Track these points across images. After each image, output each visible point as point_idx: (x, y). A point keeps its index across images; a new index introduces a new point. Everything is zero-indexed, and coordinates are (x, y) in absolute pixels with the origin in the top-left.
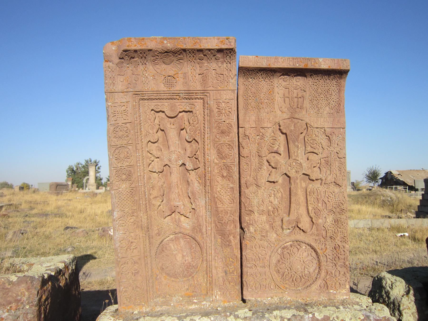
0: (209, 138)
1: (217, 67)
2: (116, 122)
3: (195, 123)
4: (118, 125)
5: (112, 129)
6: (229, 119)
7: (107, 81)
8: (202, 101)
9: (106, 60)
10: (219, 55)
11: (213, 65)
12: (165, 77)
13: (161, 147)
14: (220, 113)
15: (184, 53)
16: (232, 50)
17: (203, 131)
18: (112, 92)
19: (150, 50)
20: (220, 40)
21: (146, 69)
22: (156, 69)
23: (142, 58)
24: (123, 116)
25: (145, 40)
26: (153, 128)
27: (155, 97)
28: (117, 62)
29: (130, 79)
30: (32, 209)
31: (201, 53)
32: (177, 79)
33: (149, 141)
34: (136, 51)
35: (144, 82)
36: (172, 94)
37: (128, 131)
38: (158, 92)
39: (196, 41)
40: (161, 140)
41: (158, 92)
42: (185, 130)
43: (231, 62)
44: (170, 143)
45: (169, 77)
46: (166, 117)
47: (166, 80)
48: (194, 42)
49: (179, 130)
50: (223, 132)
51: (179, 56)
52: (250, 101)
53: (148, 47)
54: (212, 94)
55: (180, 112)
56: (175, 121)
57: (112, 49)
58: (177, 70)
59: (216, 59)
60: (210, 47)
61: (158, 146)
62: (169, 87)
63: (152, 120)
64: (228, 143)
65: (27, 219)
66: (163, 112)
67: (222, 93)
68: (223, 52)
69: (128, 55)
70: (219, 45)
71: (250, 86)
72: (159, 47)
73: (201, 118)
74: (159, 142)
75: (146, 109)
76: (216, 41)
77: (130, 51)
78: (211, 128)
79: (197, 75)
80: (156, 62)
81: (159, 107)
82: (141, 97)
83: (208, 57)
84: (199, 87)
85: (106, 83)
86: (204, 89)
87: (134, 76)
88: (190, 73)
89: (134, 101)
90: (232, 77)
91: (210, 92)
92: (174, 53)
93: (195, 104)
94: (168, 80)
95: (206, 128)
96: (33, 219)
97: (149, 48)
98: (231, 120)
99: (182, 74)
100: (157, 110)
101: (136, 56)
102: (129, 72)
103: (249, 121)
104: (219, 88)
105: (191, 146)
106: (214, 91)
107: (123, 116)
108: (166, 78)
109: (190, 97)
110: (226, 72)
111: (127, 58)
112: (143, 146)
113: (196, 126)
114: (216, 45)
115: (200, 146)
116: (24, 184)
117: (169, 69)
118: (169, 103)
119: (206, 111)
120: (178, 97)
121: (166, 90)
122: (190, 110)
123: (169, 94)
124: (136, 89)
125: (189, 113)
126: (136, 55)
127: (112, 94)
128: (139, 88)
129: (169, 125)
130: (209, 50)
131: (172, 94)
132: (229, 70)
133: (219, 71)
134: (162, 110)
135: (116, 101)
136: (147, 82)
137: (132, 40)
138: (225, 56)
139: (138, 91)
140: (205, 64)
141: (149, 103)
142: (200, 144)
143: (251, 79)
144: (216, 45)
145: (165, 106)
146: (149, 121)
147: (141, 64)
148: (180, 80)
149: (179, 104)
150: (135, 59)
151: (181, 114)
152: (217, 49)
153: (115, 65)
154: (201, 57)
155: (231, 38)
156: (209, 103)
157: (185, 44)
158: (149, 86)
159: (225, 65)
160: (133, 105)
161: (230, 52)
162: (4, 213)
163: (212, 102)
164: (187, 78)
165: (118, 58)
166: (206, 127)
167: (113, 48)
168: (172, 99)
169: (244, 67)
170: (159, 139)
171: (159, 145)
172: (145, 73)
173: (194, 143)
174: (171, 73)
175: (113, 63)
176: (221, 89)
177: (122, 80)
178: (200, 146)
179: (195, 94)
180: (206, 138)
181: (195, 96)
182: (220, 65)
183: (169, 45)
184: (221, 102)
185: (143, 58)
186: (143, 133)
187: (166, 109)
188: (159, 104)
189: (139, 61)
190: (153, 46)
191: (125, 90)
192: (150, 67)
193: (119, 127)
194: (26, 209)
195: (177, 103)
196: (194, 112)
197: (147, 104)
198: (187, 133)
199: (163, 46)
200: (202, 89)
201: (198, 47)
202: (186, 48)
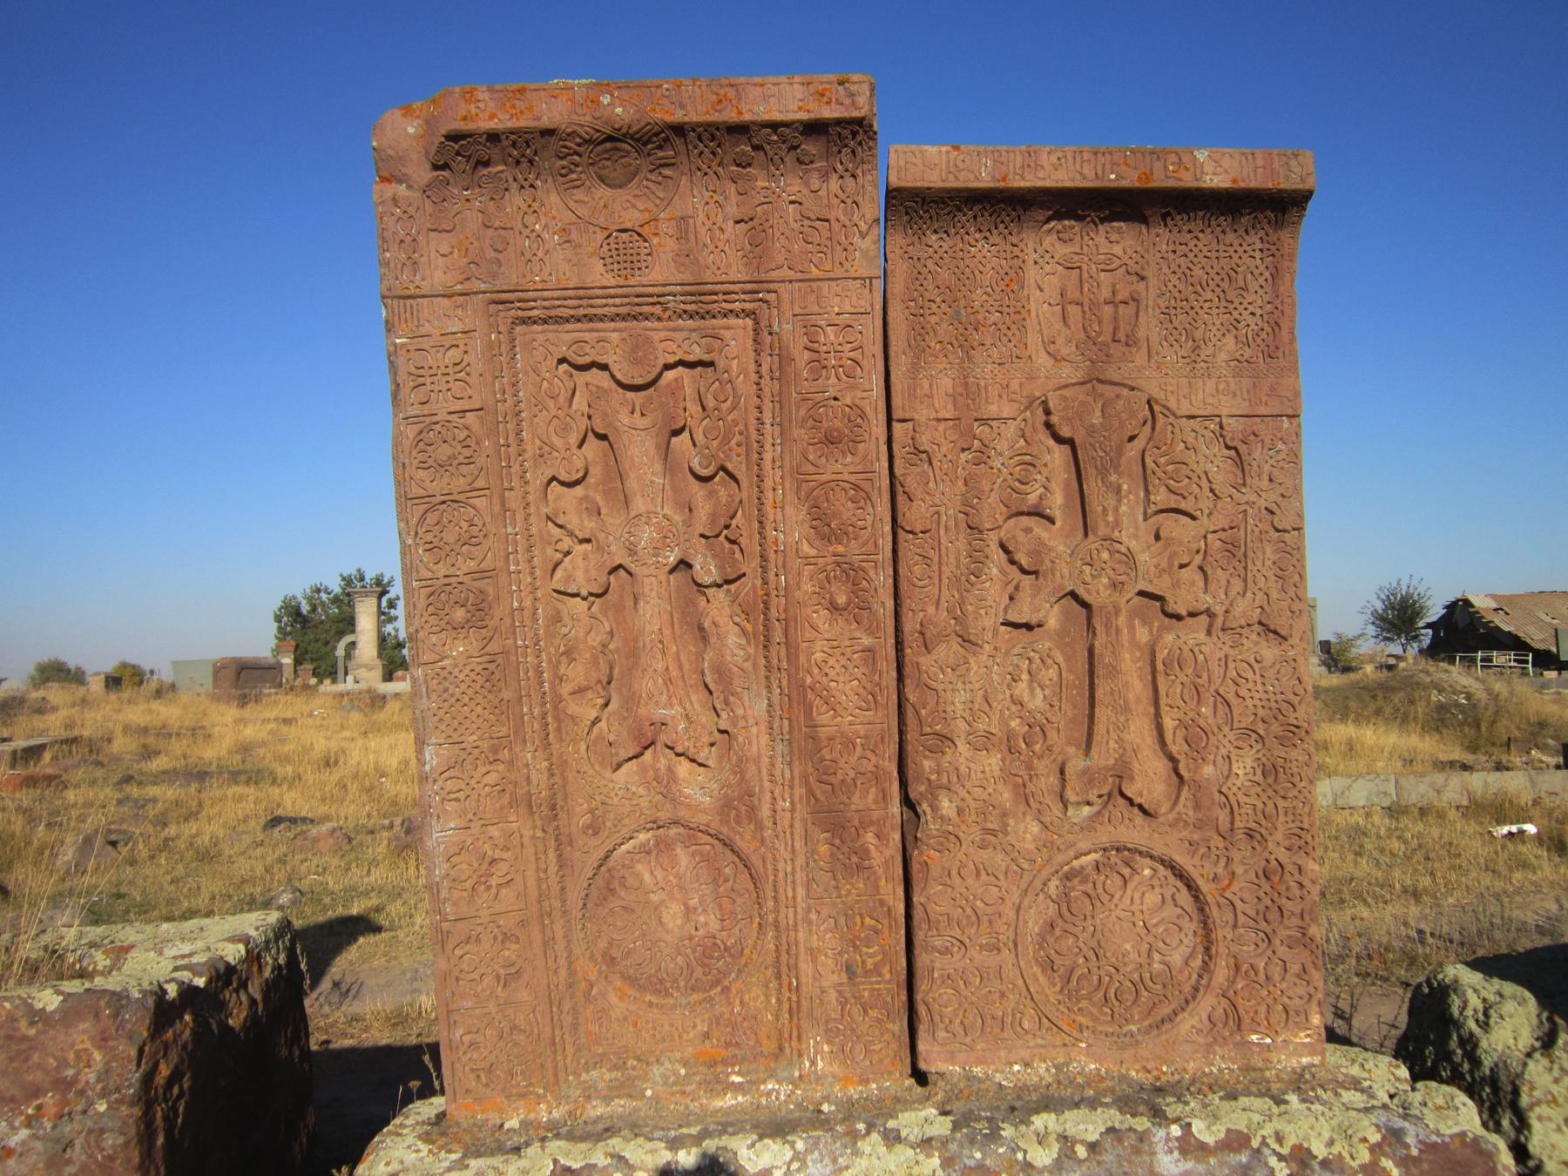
1: (805, 191)
2: (426, 410)
3: (724, 406)
4: (435, 419)
5: (411, 436)
6: (853, 387)
9: (385, 174)
10: (810, 147)
11: (791, 185)
12: (606, 234)
14: (819, 366)
15: (679, 142)
16: (861, 125)
17: (754, 435)
18: (409, 297)
19: (548, 133)
20: (812, 88)
22: (572, 204)
23: (518, 163)
26: (566, 429)
27: (572, 312)
28: (425, 182)
29: (476, 244)
30: (148, 753)
31: (744, 138)
32: (655, 241)
34: (493, 137)
35: (528, 255)
38: (581, 292)
39: (722, 92)
40: (596, 474)
41: (583, 293)
42: (686, 434)
43: (859, 172)
44: (632, 483)
46: (614, 386)
48: (715, 98)
50: (830, 440)
51: (660, 154)
53: (539, 119)
54: (786, 297)
57: (404, 131)
58: (650, 206)
60: (776, 116)
62: (623, 272)
63: (561, 399)
64: (852, 478)
65: (134, 791)
67: (825, 292)
69: (466, 154)
73: (745, 386)
74: (591, 480)
75: (540, 359)
76: (798, 91)
77: (471, 136)
78: (786, 424)
79: (731, 223)
80: (574, 176)
81: (587, 348)
82: (520, 313)
83: (770, 153)
86: (756, 276)
87: (490, 232)
88: (702, 216)
89: (491, 326)
92: (638, 140)
93: (727, 334)
94: (621, 246)
97: (546, 122)
98: (859, 394)
99: (673, 223)
100: (581, 361)
101: (495, 158)
102: (473, 218)
106: (797, 285)
108: (611, 240)
109: (702, 309)
112: (530, 498)
113: (730, 418)
114: (800, 109)
117: (624, 206)
118: (625, 335)
120: (657, 310)
121: (613, 282)
122: (706, 357)
124: (500, 284)
126: (495, 152)
127: (408, 302)
129: (625, 418)
130: (774, 126)
132: (849, 201)
134: (600, 359)
135: (423, 331)
136: (540, 254)
140: (760, 184)
143: (934, 237)
144: (800, 109)
145: (611, 343)
146: (551, 403)
147: (514, 186)
148: (666, 245)
149: (663, 334)
150: (493, 170)
151: (670, 375)
152: (801, 122)
154: (744, 153)
155: (855, 78)
156: (776, 328)
157: (682, 106)
159: (834, 184)
160: (490, 345)
161: (854, 134)
163: (790, 326)
164: (692, 237)
165: (428, 166)
167: (411, 130)
168: (635, 318)
170: (592, 471)
171: (591, 493)
172: (530, 219)
173: (722, 483)
174: (632, 218)
175: (409, 187)
176: (822, 275)
177: (445, 249)
178: (744, 495)
179: (721, 297)
180: (767, 464)
182: (815, 183)
183: (619, 110)
185: (525, 165)
186: (529, 447)
187: (615, 358)
188: (586, 336)
190: (559, 117)
191: (459, 287)
193: (438, 427)
195: (656, 332)
196: (721, 363)
197: (541, 338)
199: (597, 114)
201: (730, 115)
202: (686, 119)
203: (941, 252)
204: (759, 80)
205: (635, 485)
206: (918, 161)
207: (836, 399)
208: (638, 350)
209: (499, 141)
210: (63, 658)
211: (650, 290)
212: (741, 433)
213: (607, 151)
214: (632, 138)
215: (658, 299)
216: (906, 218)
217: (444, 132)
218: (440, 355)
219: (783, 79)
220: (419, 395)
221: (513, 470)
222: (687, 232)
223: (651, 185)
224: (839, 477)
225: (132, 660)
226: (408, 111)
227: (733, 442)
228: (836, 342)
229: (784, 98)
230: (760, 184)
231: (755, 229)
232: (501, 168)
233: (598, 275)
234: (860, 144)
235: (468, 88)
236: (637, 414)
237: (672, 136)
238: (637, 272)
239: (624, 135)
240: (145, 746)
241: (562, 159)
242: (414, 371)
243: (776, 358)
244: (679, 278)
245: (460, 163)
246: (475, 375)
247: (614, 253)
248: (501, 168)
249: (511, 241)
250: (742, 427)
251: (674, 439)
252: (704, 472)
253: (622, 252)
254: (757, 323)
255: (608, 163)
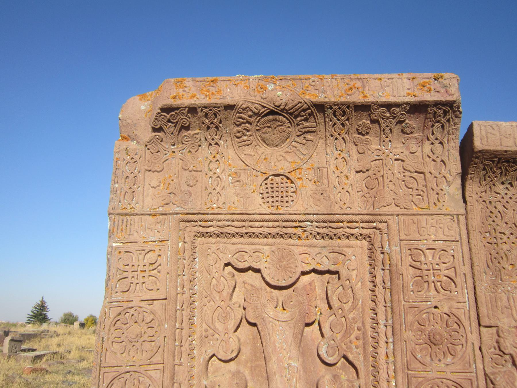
0: (391, 359)
1: (406, 152)
2: (125, 297)
3: (347, 307)
4: (131, 304)
5: (112, 316)
6: (450, 299)
7: (117, 185)
8: (365, 243)
9: (124, 135)
10: (412, 122)
11: (397, 147)
12: (265, 177)
13: (247, 372)
14: (422, 280)
15: (320, 116)
16: (451, 107)
17: (369, 331)
18: (126, 215)
19: (230, 107)
20: (416, 82)
21: (218, 157)
22: (243, 157)
23: (208, 128)
24: (145, 280)
25: (218, 83)
26: (226, 317)
27: (237, 230)
28: (147, 139)
29: (176, 181)
30: (82, 359)
31: (366, 115)
32: (299, 183)
33: (214, 355)
34: (193, 110)
35: (210, 190)
36: (284, 224)
37: (155, 324)
38: (245, 217)
39: (352, 83)
40: (246, 351)
41: (246, 217)
42: (316, 325)
43: (445, 140)
44: (273, 365)
45: (278, 179)
46: (264, 285)
47: (269, 185)
48: (347, 87)
49: (301, 324)
50: (432, 342)
51: (306, 124)
52: (505, 247)
53: (224, 98)
54: (394, 226)
55: (304, 273)
56: (290, 297)
57: (139, 109)
58: (297, 159)
59: (403, 132)
60: (392, 99)
61: (238, 372)
62: (276, 204)
63: (225, 293)
64: (454, 377)
65: (70, 377)
66: (258, 271)
67: (424, 223)
68: (426, 112)
69: (173, 120)
70: (417, 93)
71: (500, 207)
72: (254, 99)
73: (363, 293)
74: (242, 357)
75: (212, 262)
76: (407, 83)
77: (177, 109)
78: (397, 326)
79: (353, 172)
80: (245, 138)
81: (246, 257)
82: (201, 229)
83: (383, 125)
84: (358, 205)
85: (114, 191)
86: (371, 211)
87: (186, 173)
88: (332, 168)
89: (179, 237)
90: (450, 178)
91: (391, 220)
92: (291, 114)
93: (348, 251)
94: (275, 186)
95: (382, 327)
96: (77, 378)
97: (229, 101)
98: (455, 305)
99: (312, 171)
100: (241, 266)
101: (193, 124)
102: (175, 164)
103: (509, 308)
104: (415, 209)
105: (336, 377)
106: (402, 218)
107: (145, 280)
108: (268, 181)
109: (331, 232)
110: (430, 166)
111: (172, 129)
112: (195, 371)
113: (351, 316)
114: (408, 94)
115: (362, 382)
116: (91, 316)
117: (279, 158)
118: (274, 248)
119: (379, 274)
120: (299, 231)
121: (268, 211)
122: (333, 268)
123: (277, 224)
124: (189, 208)
125: (327, 276)
126: (193, 121)
127: (125, 218)
128: (197, 204)
129: (270, 311)
130: (388, 106)
131: (284, 224)
132: (438, 160)
133: (411, 163)
134: (256, 266)
135: (132, 238)
136: (218, 189)
137: (187, 84)
138: (430, 124)
139: (192, 211)
140: (374, 146)
141: (221, 246)
142: (362, 373)
143: (502, 187)
144: (408, 94)
145: (264, 254)
146: (217, 296)
147: (205, 144)
148: (306, 187)
149: (302, 249)
150: (191, 132)
151: (305, 279)
152: (409, 103)
153: (143, 147)
154: (364, 125)
155: (446, 75)
156: (386, 249)
157: (324, 92)
158: (222, 200)
159: (427, 147)
160: (177, 251)
161: (445, 113)
162: (44, 366)
163: (398, 248)
164: (325, 181)
165: (150, 129)
166: (382, 322)
167: (143, 108)
168: (282, 236)
169: (488, 151)
170: (244, 350)
171: (242, 369)
172: (214, 165)
173: (343, 368)
174: (283, 167)
175: (138, 143)
176: (420, 211)
177: (154, 183)
178: (362, 382)
179: (346, 224)
180: (382, 358)
181: (348, 230)
182: (414, 147)
183: (279, 93)
184: (423, 247)
185: (213, 130)
186: (198, 330)
187: (266, 265)
188: (246, 247)
189: (201, 136)
190: (238, 98)
191: (161, 209)
192: (229, 151)
193: (132, 311)
194: (73, 361)
195: (296, 247)
196: (344, 273)
197: (214, 247)
198: (322, 335)
199: (264, 96)
200: (366, 212)
201: (357, 98)
202: (327, 100)
203: (507, 198)
204: (378, 76)
205: (275, 366)
206: (496, 132)
207: (436, 307)
208: (283, 260)
209: (197, 112)
210: (72, 312)
211: (294, 217)
212: (359, 330)
213: (269, 121)
214: (287, 112)
215: (300, 224)
216: (483, 173)
217: (160, 106)
218: (141, 257)
219: (395, 75)
220: (123, 285)
221: (183, 349)
222: (321, 177)
223: (297, 145)
224: (443, 375)
225: (94, 315)
226: (143, 97)
227: (353, 337)
228: (434, 262)
229: (397, 87)
230: (374, 146)
231: (372, 180)
232: (197, 131)
233: (258, 205)
234: (448, 121)
235: (179, 79)
236: (280, 308)
237: (315, 111)
238: (286, 204)
239: (282, 110)
240: (80, 357)
241: (238, 126)
242: (121, 267)
243: (387, 272)
244: (316, 210)
245: (170, 128)
246: (164, 273)
247: (270, 190)
248: (197, 131)
249: (200, 180)
250: (360, 324)
251: (307, 329)
252: (330, 360)
253: (275, 189)
254: (371, 243)
255: (269, 130)
